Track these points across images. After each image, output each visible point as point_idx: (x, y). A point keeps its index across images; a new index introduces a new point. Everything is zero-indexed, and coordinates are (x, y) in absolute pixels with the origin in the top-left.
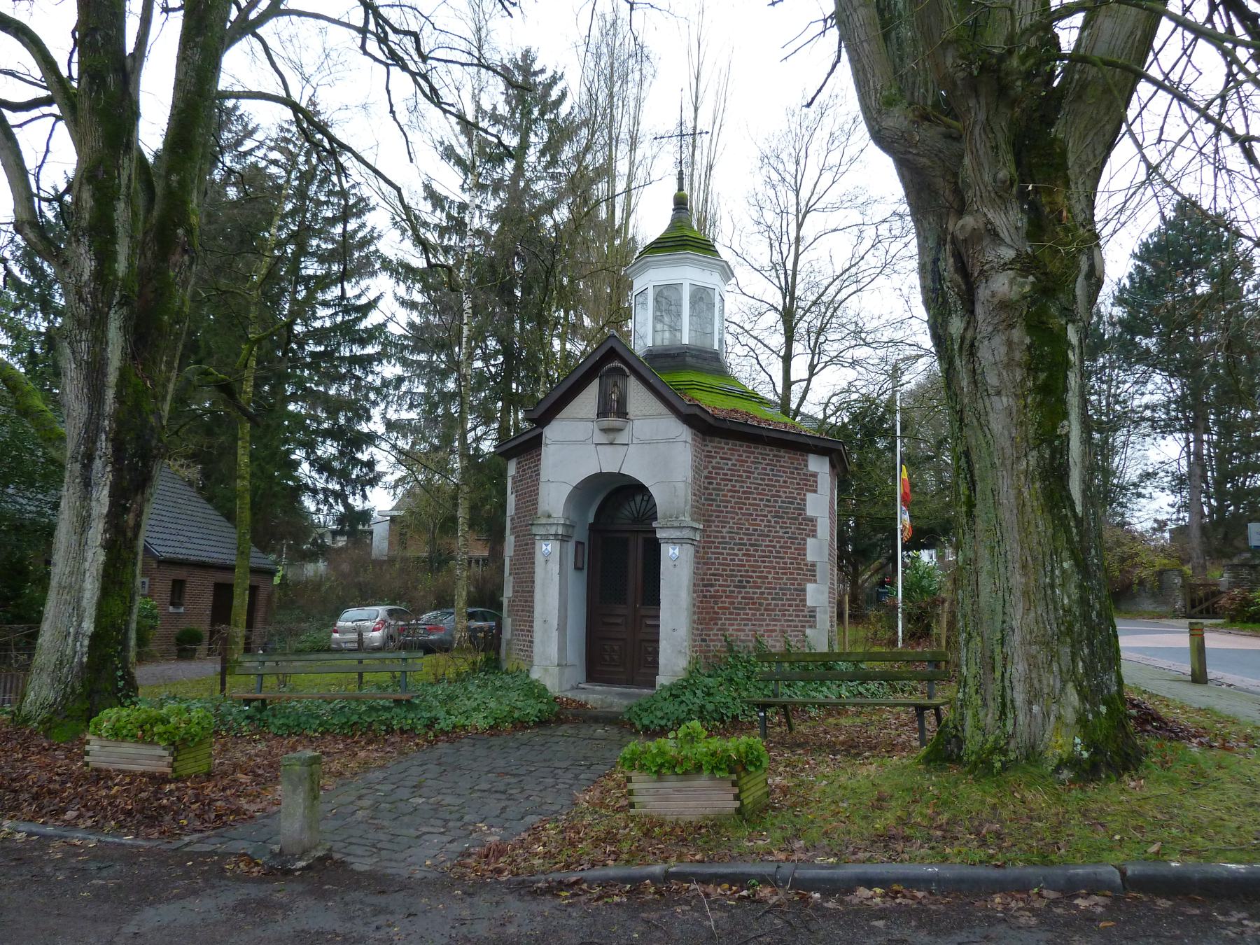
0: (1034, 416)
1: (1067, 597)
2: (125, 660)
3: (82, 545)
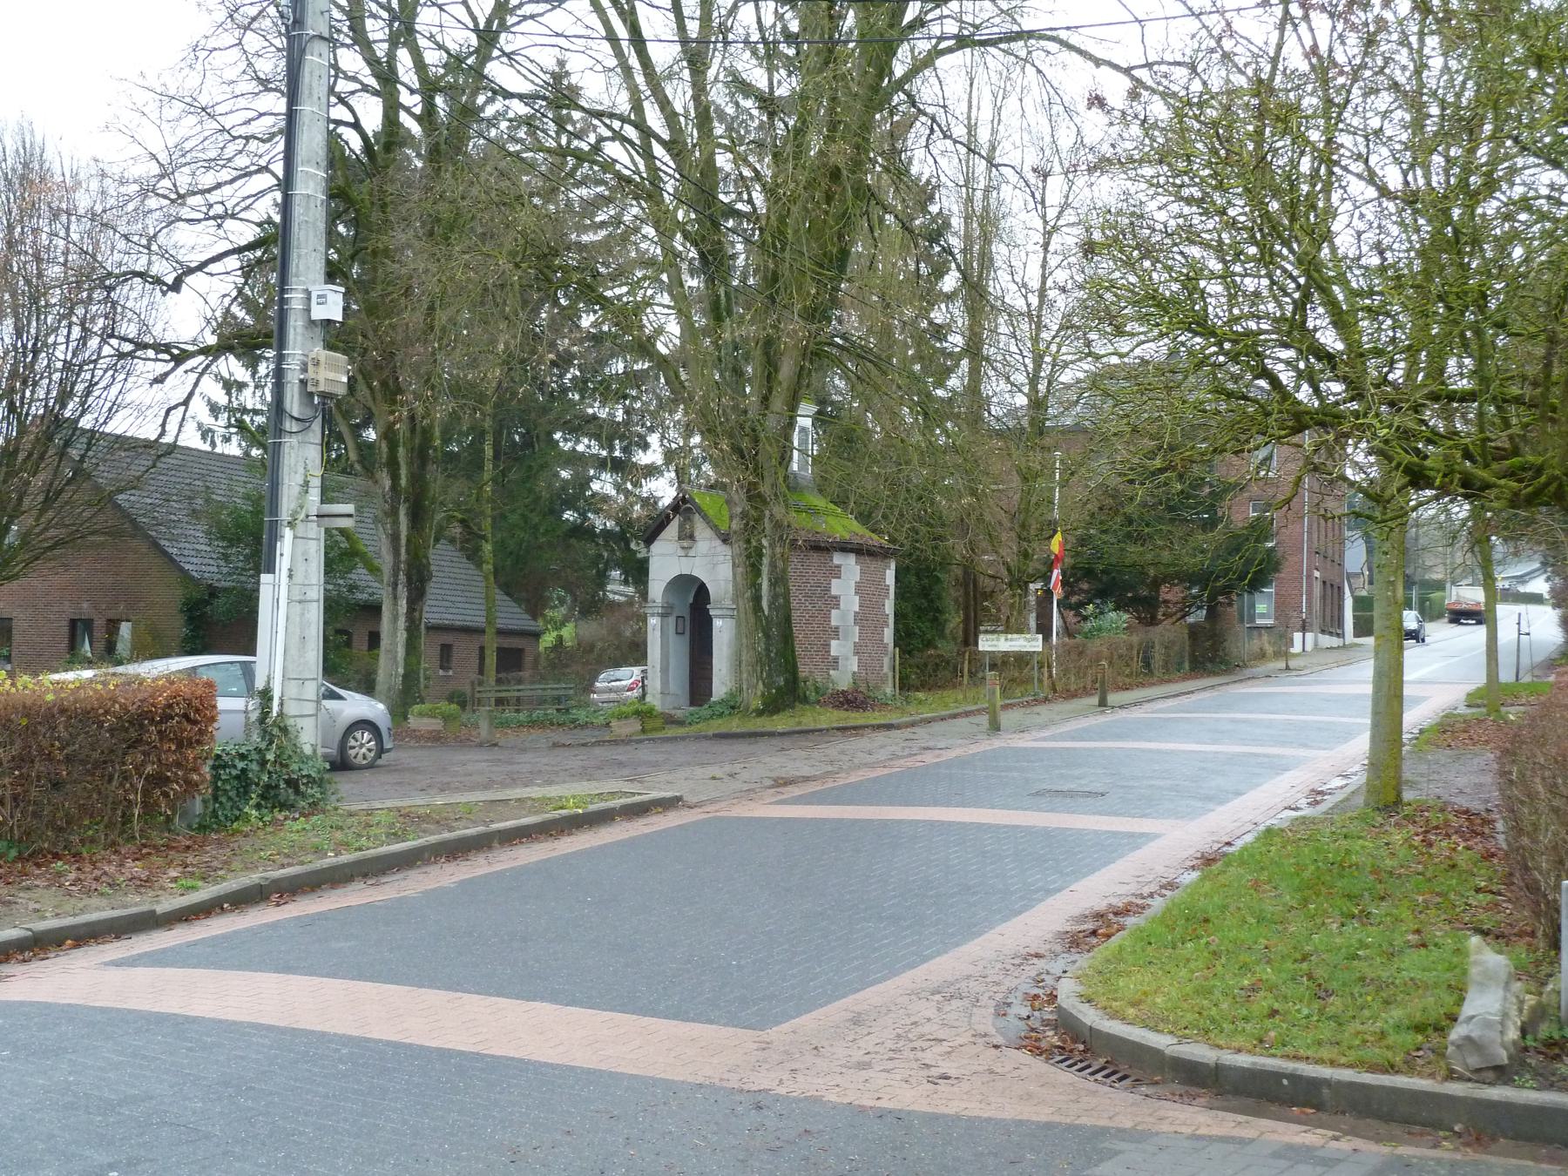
0: (750, 576)
2: (419, 688)
3: (395, 630)
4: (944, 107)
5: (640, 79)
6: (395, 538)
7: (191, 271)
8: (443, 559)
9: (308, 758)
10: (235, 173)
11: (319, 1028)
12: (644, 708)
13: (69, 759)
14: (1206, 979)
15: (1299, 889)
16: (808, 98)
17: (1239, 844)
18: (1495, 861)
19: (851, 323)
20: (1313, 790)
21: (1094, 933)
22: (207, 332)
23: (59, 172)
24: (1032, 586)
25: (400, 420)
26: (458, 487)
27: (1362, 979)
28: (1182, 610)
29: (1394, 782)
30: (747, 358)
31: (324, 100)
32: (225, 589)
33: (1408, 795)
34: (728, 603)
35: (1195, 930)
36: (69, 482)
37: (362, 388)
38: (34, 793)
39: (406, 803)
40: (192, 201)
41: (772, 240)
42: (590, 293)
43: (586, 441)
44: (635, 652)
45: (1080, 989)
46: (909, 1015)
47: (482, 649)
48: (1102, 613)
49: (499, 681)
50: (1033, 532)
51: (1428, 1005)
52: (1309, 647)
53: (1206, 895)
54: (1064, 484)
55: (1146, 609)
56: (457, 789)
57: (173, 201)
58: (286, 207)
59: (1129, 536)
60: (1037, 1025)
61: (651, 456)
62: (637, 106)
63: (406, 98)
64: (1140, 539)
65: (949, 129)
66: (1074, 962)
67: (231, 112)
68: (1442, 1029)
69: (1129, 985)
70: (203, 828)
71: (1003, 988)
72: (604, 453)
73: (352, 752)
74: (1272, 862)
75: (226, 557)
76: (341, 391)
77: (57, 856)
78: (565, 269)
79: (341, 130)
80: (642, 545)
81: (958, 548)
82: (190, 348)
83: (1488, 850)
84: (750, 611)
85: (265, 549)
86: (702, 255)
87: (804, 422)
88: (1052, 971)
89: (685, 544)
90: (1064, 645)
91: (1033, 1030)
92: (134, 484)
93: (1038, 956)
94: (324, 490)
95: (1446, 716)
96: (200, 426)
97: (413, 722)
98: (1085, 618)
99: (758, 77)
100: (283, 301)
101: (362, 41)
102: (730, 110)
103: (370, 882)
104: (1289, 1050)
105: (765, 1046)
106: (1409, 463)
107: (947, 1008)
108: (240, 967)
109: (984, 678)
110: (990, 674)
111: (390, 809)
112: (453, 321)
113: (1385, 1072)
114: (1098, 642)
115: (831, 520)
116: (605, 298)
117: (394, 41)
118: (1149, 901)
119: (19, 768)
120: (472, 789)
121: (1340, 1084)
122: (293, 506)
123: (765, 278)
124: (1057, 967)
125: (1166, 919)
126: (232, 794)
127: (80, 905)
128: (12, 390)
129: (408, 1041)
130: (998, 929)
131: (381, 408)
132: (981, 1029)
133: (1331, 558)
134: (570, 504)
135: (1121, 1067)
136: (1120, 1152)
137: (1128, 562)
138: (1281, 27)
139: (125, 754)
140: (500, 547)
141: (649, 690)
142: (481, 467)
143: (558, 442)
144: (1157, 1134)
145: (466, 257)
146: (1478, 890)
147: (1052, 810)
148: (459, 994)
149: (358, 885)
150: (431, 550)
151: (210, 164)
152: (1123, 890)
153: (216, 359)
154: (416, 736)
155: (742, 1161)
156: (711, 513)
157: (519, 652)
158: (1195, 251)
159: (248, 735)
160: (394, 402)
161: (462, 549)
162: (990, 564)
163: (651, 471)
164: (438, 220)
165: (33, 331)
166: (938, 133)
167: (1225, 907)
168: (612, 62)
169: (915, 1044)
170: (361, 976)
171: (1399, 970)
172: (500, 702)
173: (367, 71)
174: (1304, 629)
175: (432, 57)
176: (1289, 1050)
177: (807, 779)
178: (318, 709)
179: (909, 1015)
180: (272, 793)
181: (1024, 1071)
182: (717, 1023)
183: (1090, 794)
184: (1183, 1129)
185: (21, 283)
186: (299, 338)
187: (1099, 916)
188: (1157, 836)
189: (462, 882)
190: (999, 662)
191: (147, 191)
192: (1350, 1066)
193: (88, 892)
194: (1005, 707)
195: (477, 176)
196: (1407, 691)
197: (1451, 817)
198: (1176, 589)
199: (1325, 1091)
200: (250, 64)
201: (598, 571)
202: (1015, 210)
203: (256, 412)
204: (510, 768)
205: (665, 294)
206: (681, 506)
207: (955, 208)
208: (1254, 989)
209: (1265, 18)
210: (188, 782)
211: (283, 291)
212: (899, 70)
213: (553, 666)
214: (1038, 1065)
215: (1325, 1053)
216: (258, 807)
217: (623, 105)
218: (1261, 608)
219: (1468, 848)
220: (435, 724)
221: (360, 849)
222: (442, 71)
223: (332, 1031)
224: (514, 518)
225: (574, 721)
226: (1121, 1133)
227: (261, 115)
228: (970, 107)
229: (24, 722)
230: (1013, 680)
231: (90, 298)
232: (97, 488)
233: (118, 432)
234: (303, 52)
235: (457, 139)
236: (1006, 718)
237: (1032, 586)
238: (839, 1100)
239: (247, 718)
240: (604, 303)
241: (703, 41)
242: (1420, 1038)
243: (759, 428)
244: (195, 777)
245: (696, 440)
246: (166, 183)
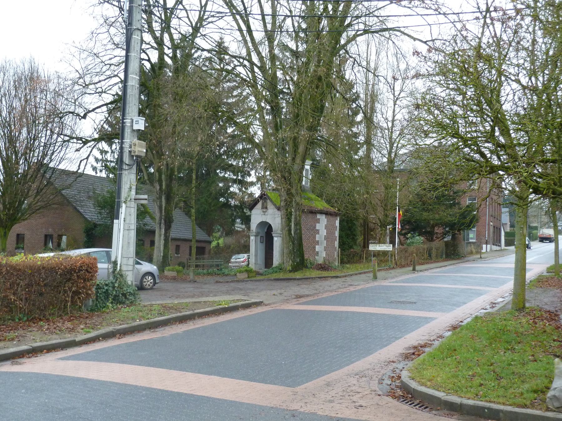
3: (160, 240)
4: (359, 55)
5: (250, 44)
6: (160, 207)
7: (90, 112)
8: (178, 215)
10: (106, 77)
11: (134, 384)
12: (249, 269)
13: (45, 285)
14: (456, 372)
15: (488, 339)
16: (310, 52)
17: (465, 322)
18: (560, 330)
19: (324, 132)
21: (414, 354)
22: (95, 133)
23: (43, 76)
24: (388, 227)
25: (163, 165)
26: (183, 190)
27: (513, 373)
29: (522, 300)
30: (286, 144)
31: (139, 51)
32: (100, 225)
33: (527, 305)
34: (279, 232)
36: (45, 186)
37: (149, 153)
38: (33, 297)
40: (91, 87)
41: (297, 102)
42: (231, 120)
43: (228, 173)
44: (246, 249)
45: (409, 374)
46: (347, 383)
47: (191, 247)
48: (413, 237)
49: (197, 259)
50: (389, 208)
51: (539, 383)
52: (488, 250)
53: (454, 341)
54: (400, 190)
55: (430, 236)
56: (182, 298)
57: (84, 87)
59: (424, 209)
60: (394, 387)
61: (252, 178)
62: (249, 54)
63: (166, 51)
64: (428, 210)
66: (407, 364)
68: (544, 392)
69: (428, 373)
70: (92, 310)
71: (381, 374)
72: (235, 177)
73: (145, 284)
74: (478, 329)
75: (100, 213)
76: (143, 155)
77: (41, 320)
78: (223, 112)
80: (248, 210)
81: (361, 212)
82: (89, 139)
83: (557, 326)
84: (287, 234)
85: (115, 211)
86: (272, 107)
87: (307, 167)
90: (400, 248)
91: (392, 389)
92: (69, 186)
93: (393, 362)
95: (540, 276)
96: (92, 166)
97: (166, 273)
98: (407, 239)
99: (292, 45)
100: (123, 123)
101: (151, 30)
102: (281, 56)
104: (487, 399)
105: (295, 394)
106: (534, 185)
107: (361, 381)
109: (371, 260)
110: (373, 259)
111: (159, 305)
112: (182, 130)
113: (524, 408)
115: (317, 202)
116: (237, 122)
117: (162, 31)
118: (433, 342)
119: (28, 288)
120: (188, 297)
121: (507, 411)
122: (126, 195)
123: (294, 116)
124: (400, 366)
125: (440, 349)
127: (49, 337)
128: (26, 153)
129: (166, 389)
130: (379, 352)
131: (156, 161)
132: (373, 388)
133: (497, 218)
134: (222, 195)
137: (423, 218)
138: (483, 27)
139: (65, 283)
140: (198, 211)
141: (250, 263)
142: (191, 182)
145: (188, 107)
146: (554, 340)
147: (397, 308)
148: (185, 372)
149: (148, 332)
150: (173, 212)
151: (97, 74)
152: (424, 338)
153: (98, 143)
154: (167, 278)
156: (273, 199)
157: (203, 248)
158: (455, 108)
159: (109, 277)
160: (161, 159)
161: (184, 211)
162: (373, 218)
163: (252, 184)
164: (177, 94)
165: (34, 132)
166: (356, 65)
168: (240, 38)
169: (350, 394)
170: (149, 365)
171: (527, 370)
173: (153, 41)
174: (487, 243)
175: (176, 36)
176: (487, 399)
177: (308, 296)
178: (133, 268)
179: (347, 383)
180: (117, 298)
181: (390, 405)
182: (278, 385)
183: (410, 303)
185: (30, 115)
186: (129, 136)
187: (415, 347)
188: (436, 318)
189: (184, 331)
190: (377, 254)
191: (75, 83)
192: (510, 405)
193: (52, 333)
194: (379, 270)
195: (192, 78)
196: (528, 266)
197: (543, 313)
198: (440, 228)
199: (501, 414)
200: (112, 39)
201: (232, 220)
202: (384, 92)
203: (111, 162)
204: (201, 290)
205: (257, 121)
206: (263, 197)
207: (362, 91)
208: (473, 376)
209: (477, 24)
210: (87, 294)
211: (123, 119)
212: (343, 42)
213: (216, 253)
214: (395, 402)
215: (501, 400)
216: (112, 303)
217: (244, 53)
218: (471, 236)
219: (550, 325)
220: (174, 274)
221: (148, 319)
223: (139, 385)
224: (203, 200)
225: (223, 273)
227: (115, 56)
228: (367, 55)
229: (30, 272)
230: (381, 261)
231: (54, 120)
232: (55, 188)
233: (63, 168)
234: (132, 34)
235: (185, 66)
236: (379, 274)
237: (388, 227)
238: (323, 414)
239: (108, 271)
240: (236, 124)
241: (273, 31)
242: (536, 395)
243: (291, 169)
244: (90, 292)
245: (268, 173)
246: (81, 80)
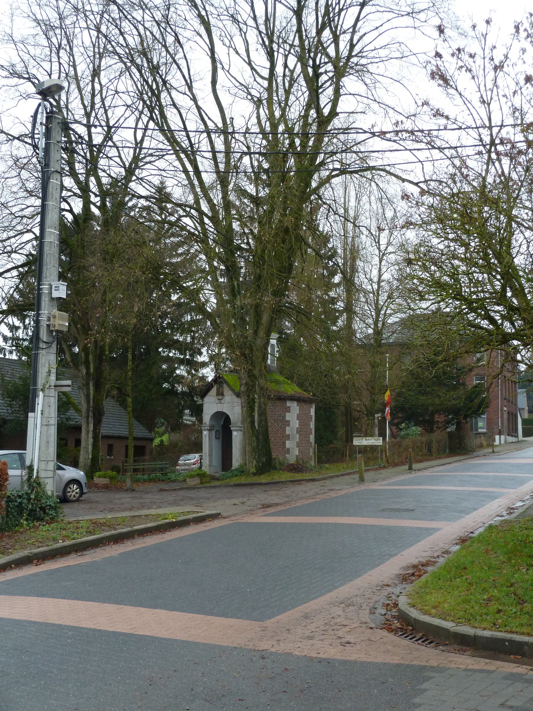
1: (254, 444)
3: (88, 438)
4: (335, 200)
5: (198, 190)
9: (50, 497)
11: (58, 623)
12: (201, 472)
15: (506, 553)
17: (477, 533)
19: (293, 297)
20: (509, 508)
21: (413, 575)
24: (376, 415)
28: (444, 426)
30: (247, 313)
34: (239, 424)
35: (460, 573)
37: (73, 328)
39: (94, 517)
44: (197, 447)
45: (409, 601)
48: (408, 427)
49: (135, 461)
52: (502, 442)
53: (464, 556)
54: (390, 369)
56: (117, 511)
58: (40, 247)
59: (420, 392)
60: (389, 617)
61: (204, 358)
62: (197, 202)
63: (93, 198)
64: (425, 393)
65: (337, 210)
66: (405, 588)
67: (15, 205)
71: (373, 601)
72: (182, 357)
73: (69, 494)
75: (10, 406)
76: (65, 329)
78: (165, 274)
79: (64, 213)
81: (342, 397)
87: (273, 342)
88: (395, 592)
89: (220, 398)
91: (388, 620)
93: (388, 585)
94: (57, 374)
97: (96, 480)
98: (401, 430)
99: (251, 189)
101: (73, 174)
102: (238, 203)
103: (79, 554)
104: (508, 628)
105: (265, 629)
107: (347, 610)
108: (20, 594)
109: (356, 458)
110: (359, 456)
112: (114, 297)
114: (408, 440)
117: (88, 174)
118: (437, 560)
122: (43, 382)
123: (255, 277)
124: (397, 591)
126: (15, 514)
130: (369, 573)
132: (364, 620)
133: (512, 401)
134: (166, 380)
135: (429, 637)
136: (433, 677)
138: (488, 164)
141: (204, 464)
142: (126, 363)
143: (160, 352)
144: (449, 669)
145: (121, 269)
147: (390, 518)
148: (122, 606)
149: (73, 555)
152: (425, 554)
154: (96, 486)
155: (257, 684)
156: (231, 384)
157: (144, 448)
158: (456, 262)
159: (22, 487)
160: (87, 334)
161: (117, 401)
162: (358, 405)
164: (108, 253)
167: (473, 562)
169: (334, 628)
172: (135, 470)
173: (76, 187)
174: (500, 434)
176: (508, 628)
177: (277, 505)
179: (330, 614)
180: (33, 513)
181: (385, 640)
182: (242, 618)
184: (461, 666)
186: (47, 306)
187: (415, 567)
188: (439, 529)
189: (121, 553)
194: (366, 471)
198: (442, 416)
199: (526, 648)
200: (24, 184)
203: (24, 340)
204: (141, 501)
207: (339, 246)
208: (489, 600)
212: (314, 184)
214: (391, 637)
216: (27, 520)
218: (480, 424)
220: (106, 481)
221: (74, 539)
222: (109, 187)
226: (433, 669)
227: (28, 207)
234: (49, 178)
235: (117, 217)
237: (376, 415)
238: (300, 654)
239: (22, 479)
240: (183, 289)
241: (227, 172)
245: (224, 350)
